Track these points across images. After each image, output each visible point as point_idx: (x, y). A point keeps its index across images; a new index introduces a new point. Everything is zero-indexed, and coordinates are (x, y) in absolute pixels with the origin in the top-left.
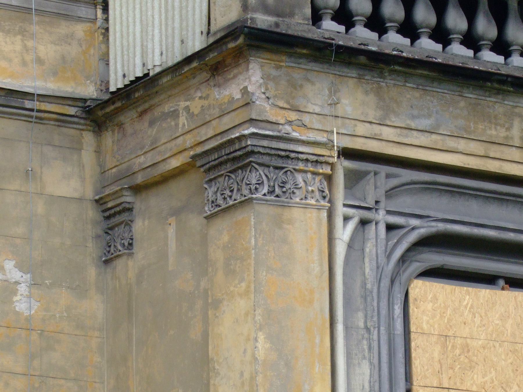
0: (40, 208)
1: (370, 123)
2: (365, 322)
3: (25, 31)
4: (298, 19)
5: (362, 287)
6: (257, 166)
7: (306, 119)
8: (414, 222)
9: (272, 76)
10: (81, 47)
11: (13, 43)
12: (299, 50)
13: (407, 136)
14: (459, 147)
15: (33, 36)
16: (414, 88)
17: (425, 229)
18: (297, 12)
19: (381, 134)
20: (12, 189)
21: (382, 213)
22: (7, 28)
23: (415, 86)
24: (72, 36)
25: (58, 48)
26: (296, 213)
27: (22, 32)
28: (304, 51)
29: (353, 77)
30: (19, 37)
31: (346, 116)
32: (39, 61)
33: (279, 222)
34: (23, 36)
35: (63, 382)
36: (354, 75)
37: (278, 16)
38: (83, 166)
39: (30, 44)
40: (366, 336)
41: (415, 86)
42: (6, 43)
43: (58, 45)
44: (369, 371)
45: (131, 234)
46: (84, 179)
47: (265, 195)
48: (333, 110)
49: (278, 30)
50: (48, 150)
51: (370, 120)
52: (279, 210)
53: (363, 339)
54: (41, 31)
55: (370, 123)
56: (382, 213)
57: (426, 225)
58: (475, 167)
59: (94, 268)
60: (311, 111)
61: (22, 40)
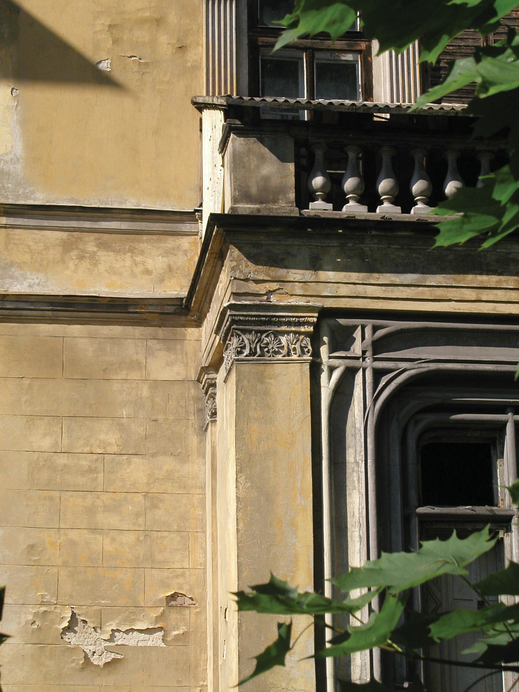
0: (145, 391)
1: (354, 284)
2: (355, 458)
3: (135, 248)
4: (282, 204)
5: (353, 427)
6: (239, 333)
7: (288, 287)
8: (404, 365)
9: (252, 255)
10: (187, 256)
11: (123, 260)
12: (273, 229)
13: (392, 291)
14: (448, 295)
15: (142, 252)
16: (398, 249)
17: (416, 370)
18: (280, 198)
19: (366, 292)
20: (119, 378)
21: (368, 361)
22: (118, 248)
23: (399, 247)
24: (178, 248)
25: (165, 259)
26: (278, 368)
27: (132, 250)
28: (277, 229)
29: (335, 246)
30: (129, 254)
31: (329, 281)
32: (148, 272)
33: (261, 379)
34: (133, 253)
35: (166, 534)
36: (336, 245)
37: (261, 203)
38: (186, 354)
39: (138, 259)
40: (356, 469)
41: (399, 247)
42: (117, 260)
43: (165, 257)
44: (358, 499)
45: (214, 405)
46: (187, 364)
47: (246, 356)
48: (314, 277)
49: (260, 214)
50: (152, 344)
51: (352, 281)
52: (262, 367)
53: (353, 471)
54: (149, 247)
55: (354, 284)
56: (368, 361)
57: (416, 366)
58: (467, 311)
59: (196, 437)
60: (292, 280)
61: (132, 257)
